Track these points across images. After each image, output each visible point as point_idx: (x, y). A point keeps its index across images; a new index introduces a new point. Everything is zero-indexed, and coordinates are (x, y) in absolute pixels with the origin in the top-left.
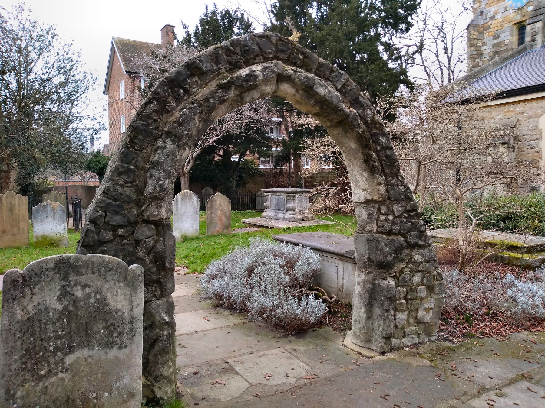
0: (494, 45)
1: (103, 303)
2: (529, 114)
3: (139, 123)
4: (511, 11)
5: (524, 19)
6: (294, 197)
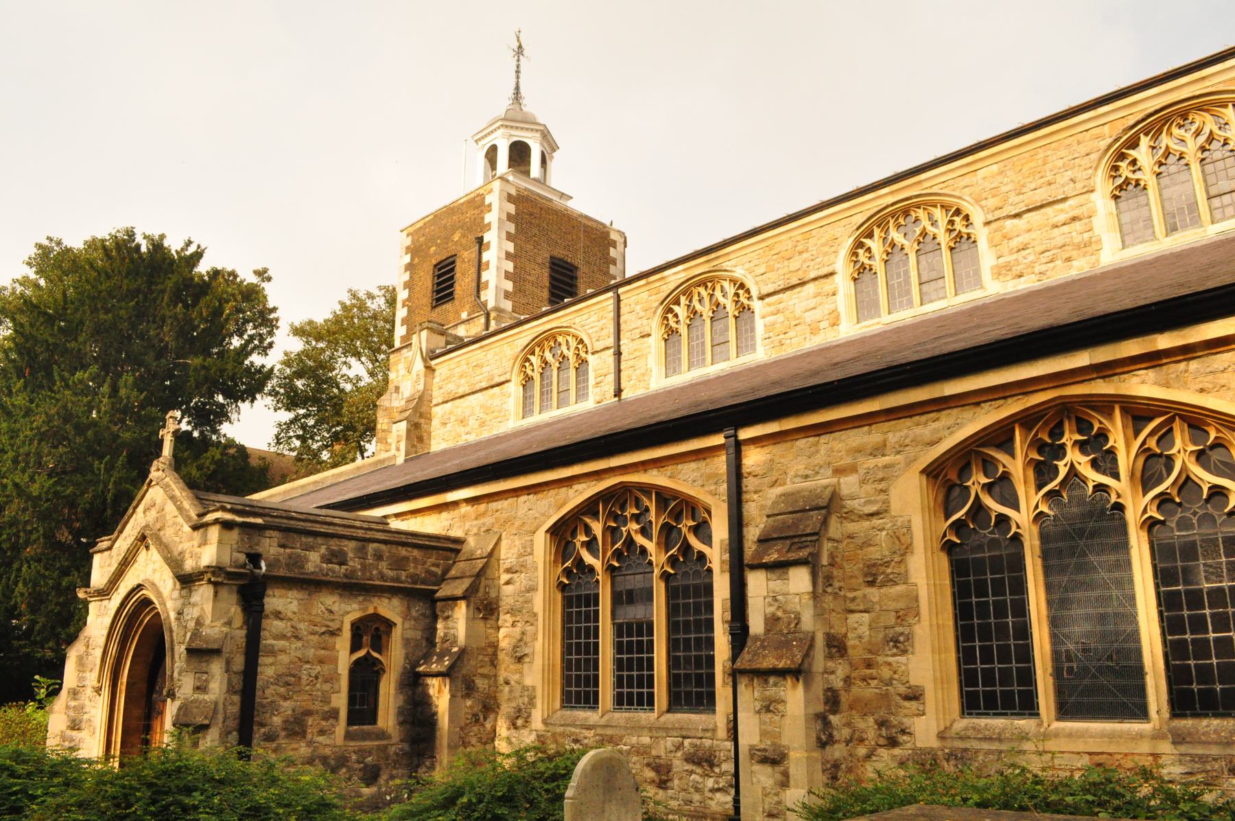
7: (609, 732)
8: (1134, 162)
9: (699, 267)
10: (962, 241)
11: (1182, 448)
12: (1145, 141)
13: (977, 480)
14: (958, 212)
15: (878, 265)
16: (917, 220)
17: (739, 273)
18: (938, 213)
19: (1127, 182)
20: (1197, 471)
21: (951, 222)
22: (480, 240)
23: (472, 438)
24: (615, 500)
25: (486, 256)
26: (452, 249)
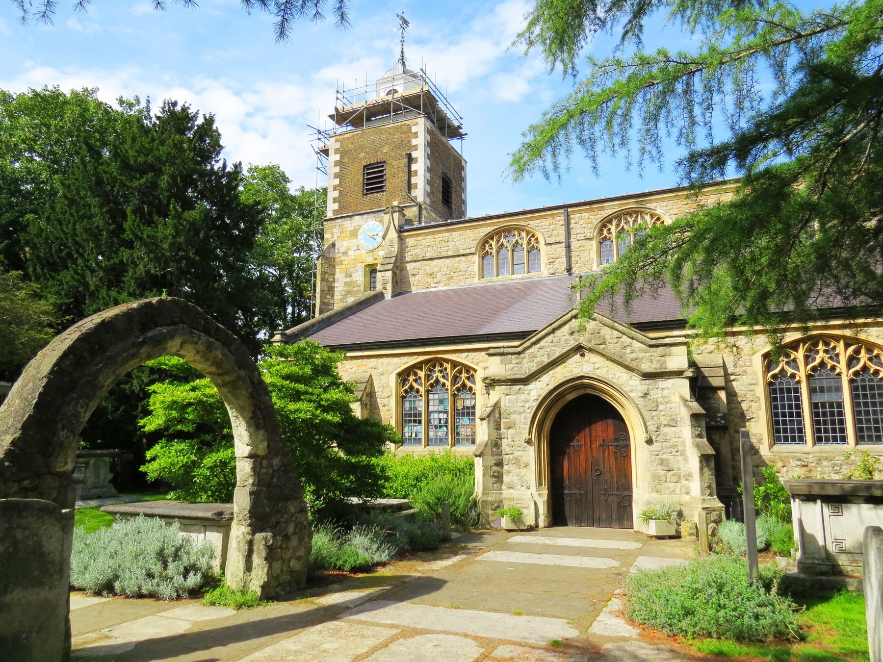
0: (346, 284)
1: (39, 545)
2: (380, 370)
3: (626, 493)
4: (363, 251)
5: (375, 262)
6: (87, 463)
7: (824, 455)
8: (609, 229)
9: (631, 204)
10: (533, 249)
11: (864, 356)
12: (614, 222)
13: (412, 378)
14: (533, 236)
15: (614, 237)
16: (514, 235)
17: (659, 211)
18: (524, 234)
19: (606, 237)
20: (467, 382)
21: (530, 240)
22: (409, 156)
23: (441, 288)
24: (433, 363)
25: (414, 167)
26: (380, 157)
